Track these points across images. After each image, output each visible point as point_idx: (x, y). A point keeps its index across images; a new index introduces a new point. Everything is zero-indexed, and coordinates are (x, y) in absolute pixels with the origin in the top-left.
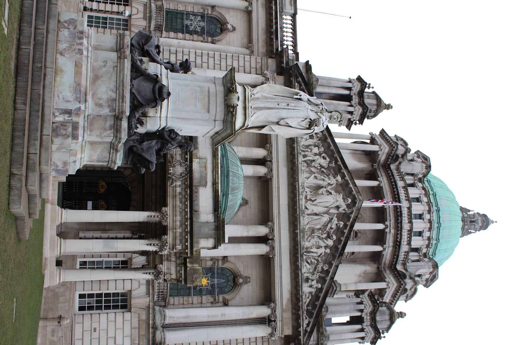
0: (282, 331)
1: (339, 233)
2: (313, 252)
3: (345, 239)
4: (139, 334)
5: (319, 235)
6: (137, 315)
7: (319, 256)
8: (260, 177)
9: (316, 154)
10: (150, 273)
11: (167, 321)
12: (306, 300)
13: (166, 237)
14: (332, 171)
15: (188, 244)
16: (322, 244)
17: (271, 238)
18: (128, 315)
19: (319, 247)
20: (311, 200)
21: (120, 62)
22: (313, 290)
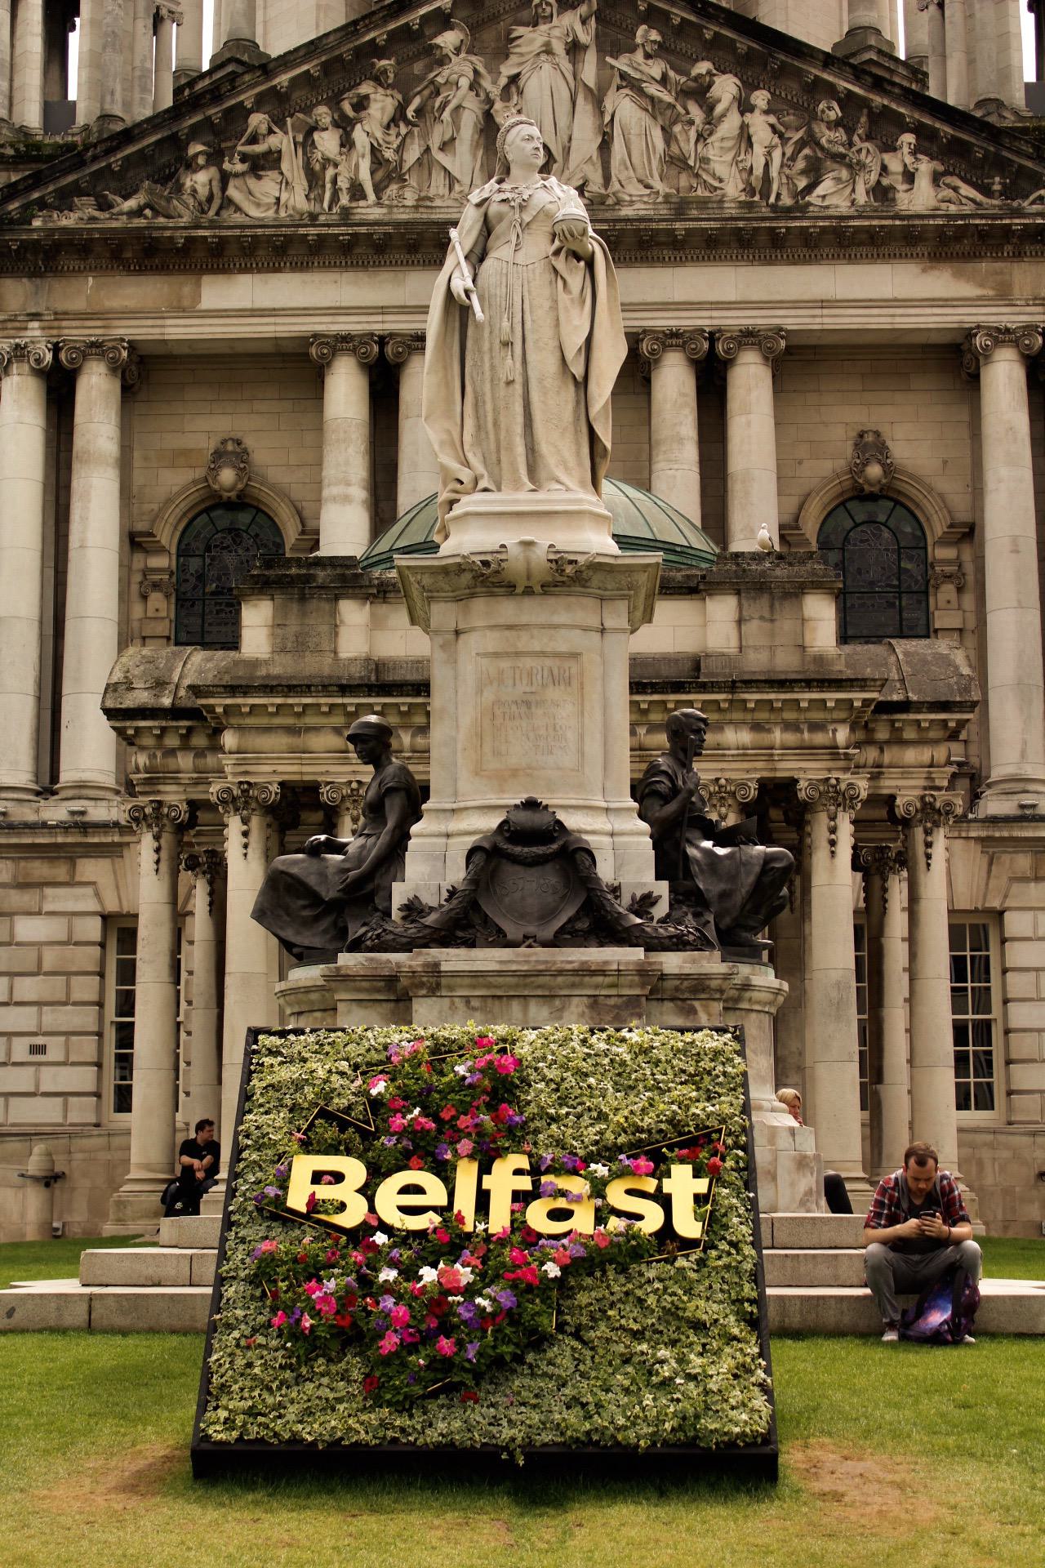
1: (682, 45)
2: (767, 166)
5: (693, 135)
6: (1016, 888)
7: (781, 136)
9: (347, 143)
10: (929, 845)
13: (802, 784)
14: (418, 68)
15: (831, 697)
16: (730, 126)
17: (706, 345)
18: (1015, 923)
19: (745, 138)
21: (451, 988)
22: (925, 167)
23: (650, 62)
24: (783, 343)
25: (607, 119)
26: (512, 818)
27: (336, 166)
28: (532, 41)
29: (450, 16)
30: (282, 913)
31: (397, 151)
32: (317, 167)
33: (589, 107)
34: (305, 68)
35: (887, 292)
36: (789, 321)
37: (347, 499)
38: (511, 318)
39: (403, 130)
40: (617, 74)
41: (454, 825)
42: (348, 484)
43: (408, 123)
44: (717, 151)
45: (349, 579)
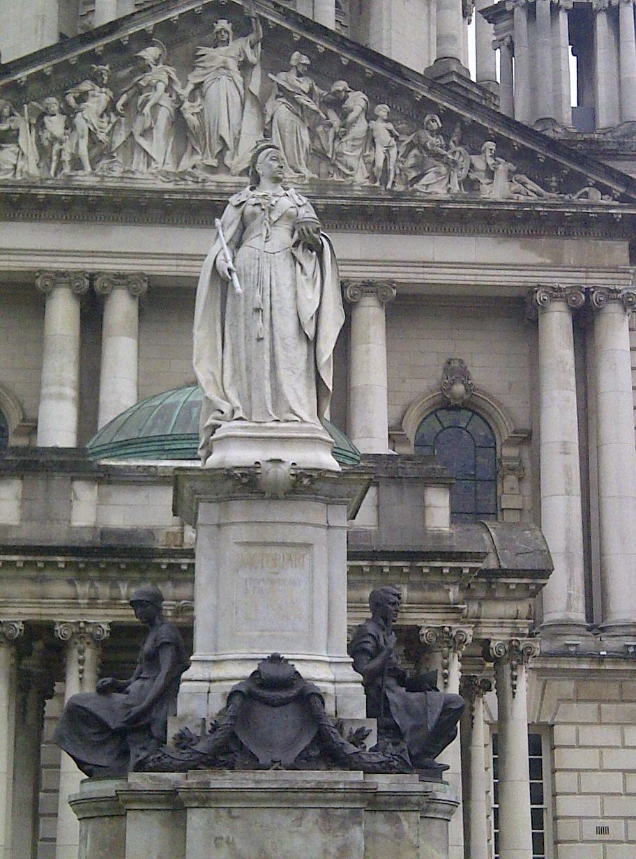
0: (616, 269)
2: (385, 160)
3: (348, 50)
4: (616, 701)
5: (331, 134)
6: (562, 706)
7: (396, 138)
8: (141, 313)
9: (70, 126)
10: (515, 678)
11: (579, 615)
12: (529, 192)
13: (424, 631)
14: (123, 73)
16: (360, 128)
18: (563, 734)
20: (221, 155)
21: (217, 800)
22: (503, 167)
23: (301, 79)
24: (395, 292)
25: (268, 119)
26: (264, 671)
27: (61, 143)
28: (213, 59)
29: (151, 36)
30: (76, 737)
31: (109, 134)
32: (46, 143)
33: (254, 110)
34: (40, 68)
35: (471, 258)
36: (400, 275)
37: (61, 397)
38: (262, 291)
39: (114, 119)
40: (276, 86)
41: (216, 672)
42: (62, 385)
43: (117, 114)
44: (349, 148)
45: (75, 465)
